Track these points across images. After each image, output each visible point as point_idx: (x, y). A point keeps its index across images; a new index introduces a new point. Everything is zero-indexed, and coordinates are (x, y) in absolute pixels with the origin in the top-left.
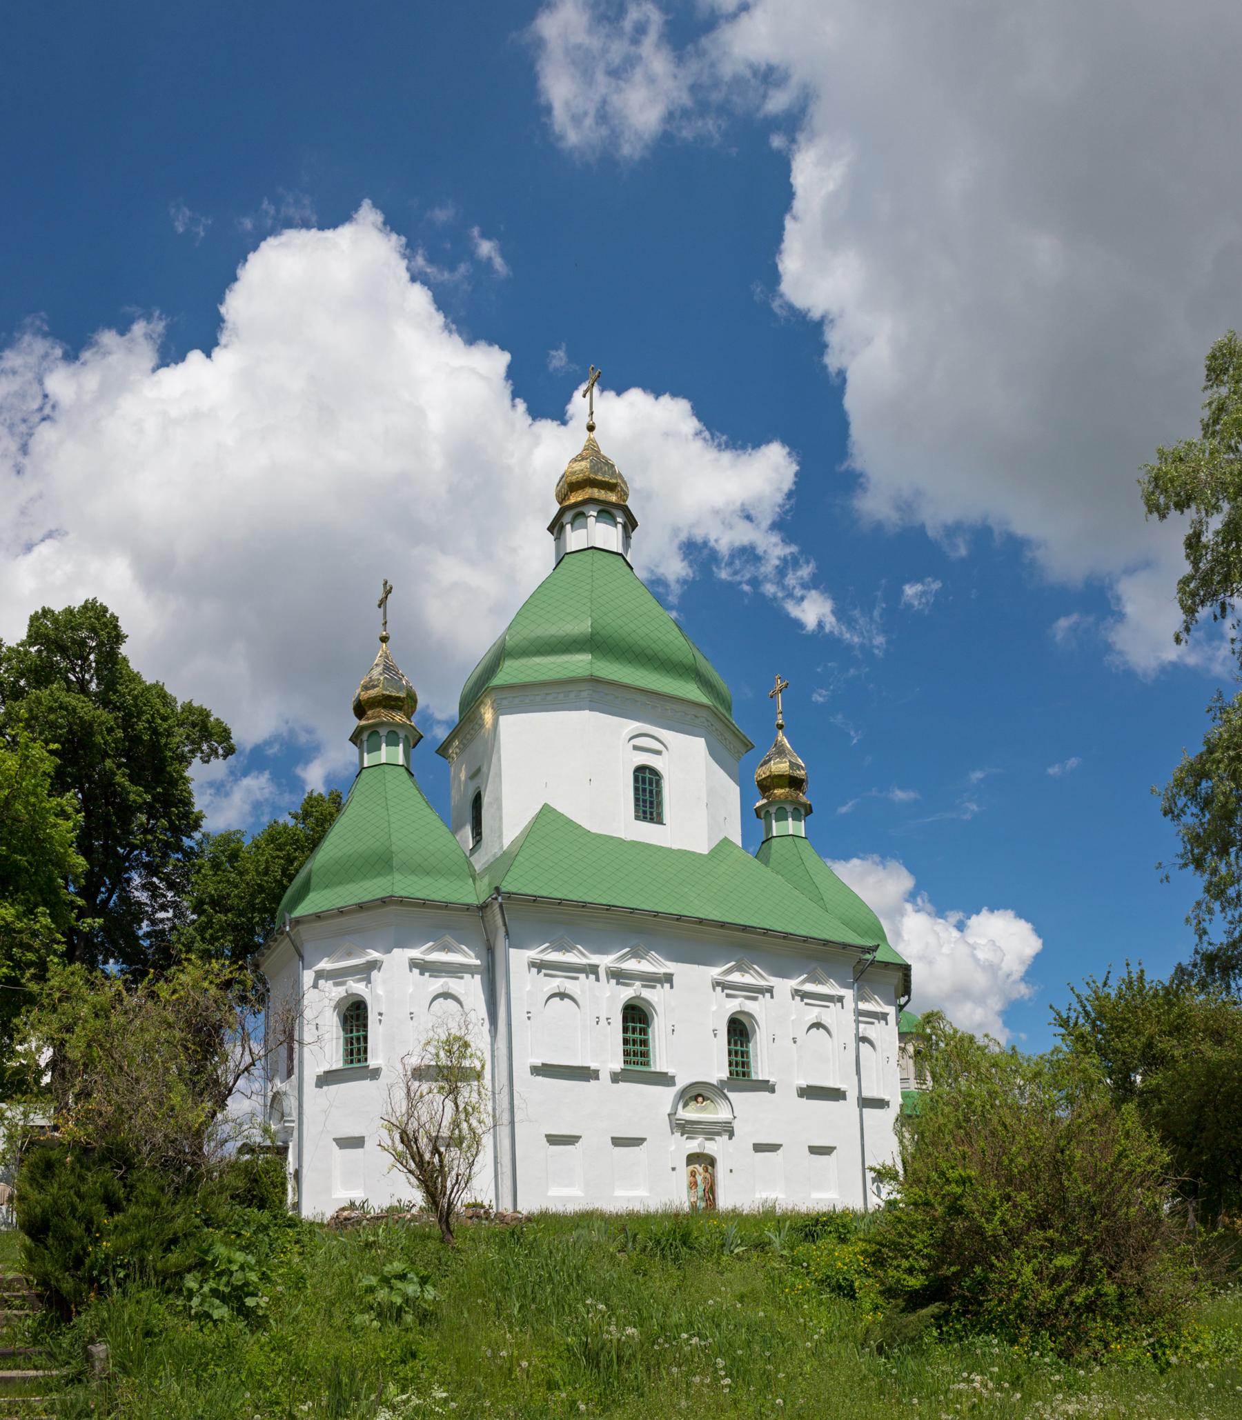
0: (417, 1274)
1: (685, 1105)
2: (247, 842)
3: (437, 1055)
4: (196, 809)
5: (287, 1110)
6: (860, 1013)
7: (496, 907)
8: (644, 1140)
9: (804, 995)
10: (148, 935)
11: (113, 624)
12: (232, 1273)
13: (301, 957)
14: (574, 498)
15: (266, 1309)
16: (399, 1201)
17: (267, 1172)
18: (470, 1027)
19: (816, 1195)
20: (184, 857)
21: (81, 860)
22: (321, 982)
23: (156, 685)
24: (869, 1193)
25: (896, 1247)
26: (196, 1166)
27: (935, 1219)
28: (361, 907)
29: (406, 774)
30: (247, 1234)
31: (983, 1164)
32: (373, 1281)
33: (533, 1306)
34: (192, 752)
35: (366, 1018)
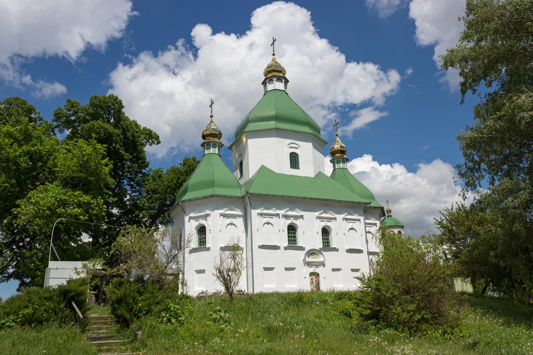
1: (308, 257)
2: (165, 171)
4: (147, 160)
6: (366, 224)
7: (247, 197)
9: (347, 219)
11: (120, 102)
13: (185, 212)
14: (269, 75)
22: (191, 220)
23: (134, 121)
28: (205, 197)
29: (218, 156)
30: (177, 300)
34: (146, 142)
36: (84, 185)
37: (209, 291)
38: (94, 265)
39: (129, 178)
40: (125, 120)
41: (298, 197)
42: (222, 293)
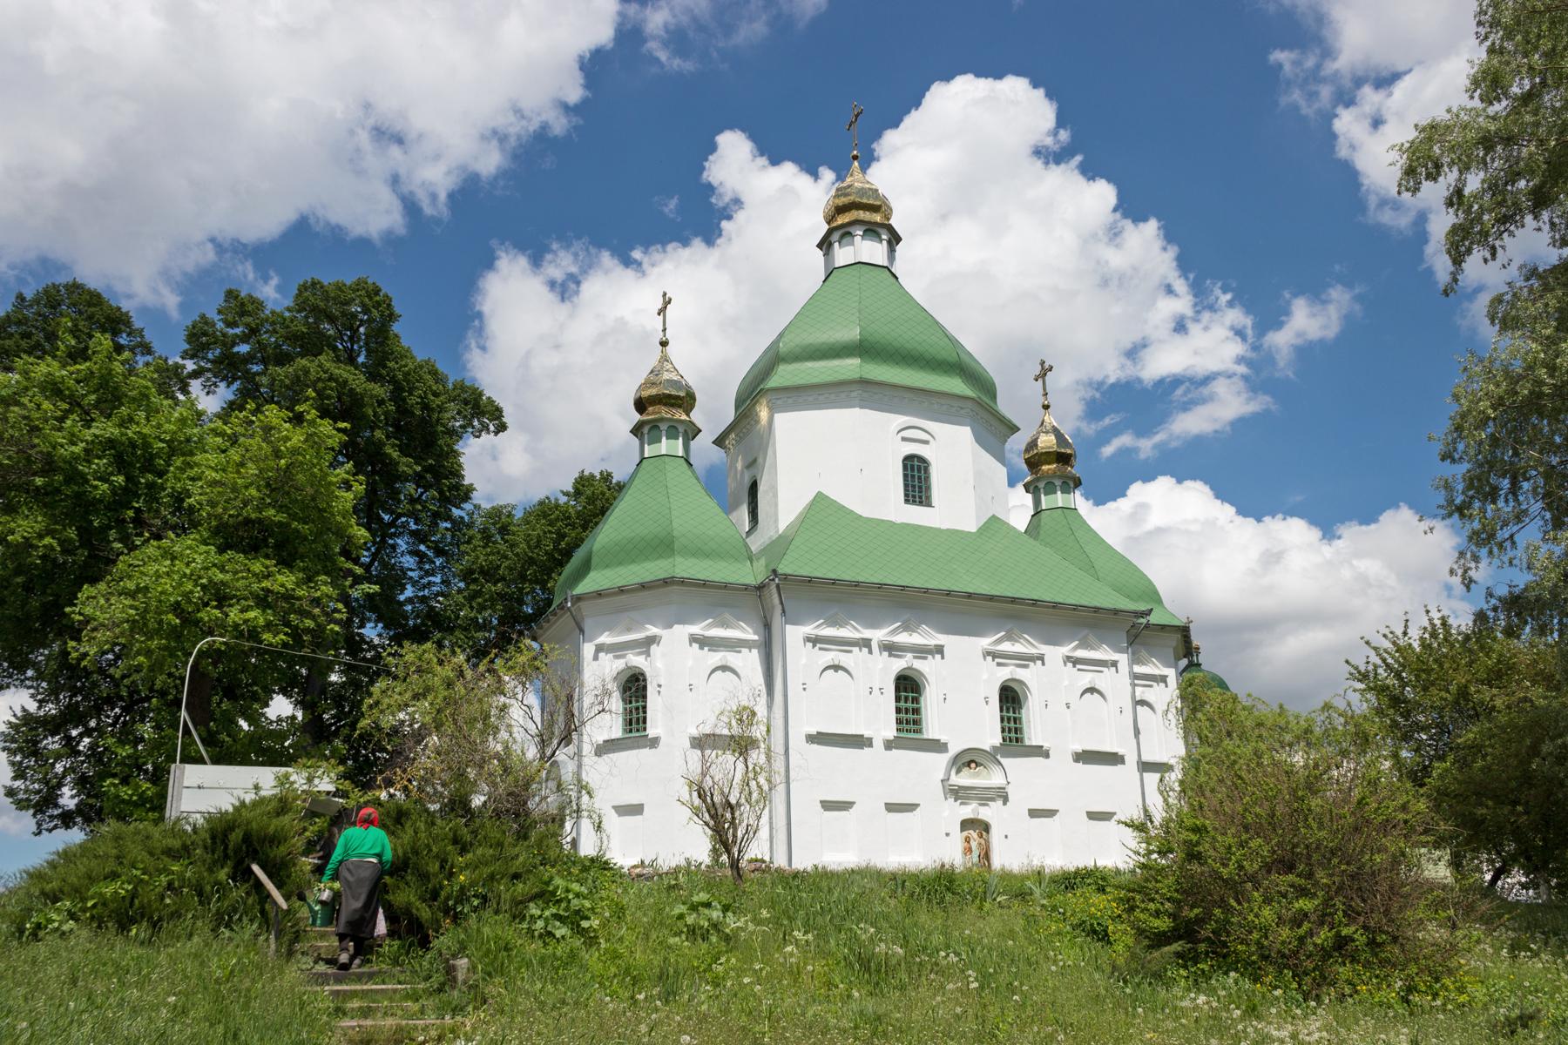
1: (958, 771)
2: (518, 514)
4: (466, 482)
6: (1136, 676)
9: (1076, 661)
13: (582, 631)
14: (841, 220)
21: (363, 532)
28: (643, 586)
36: (279, 547)
37: (660, 861)
38: (310, 780)
39: (413, 533)
40: (402, 357)
41: (927, 590)
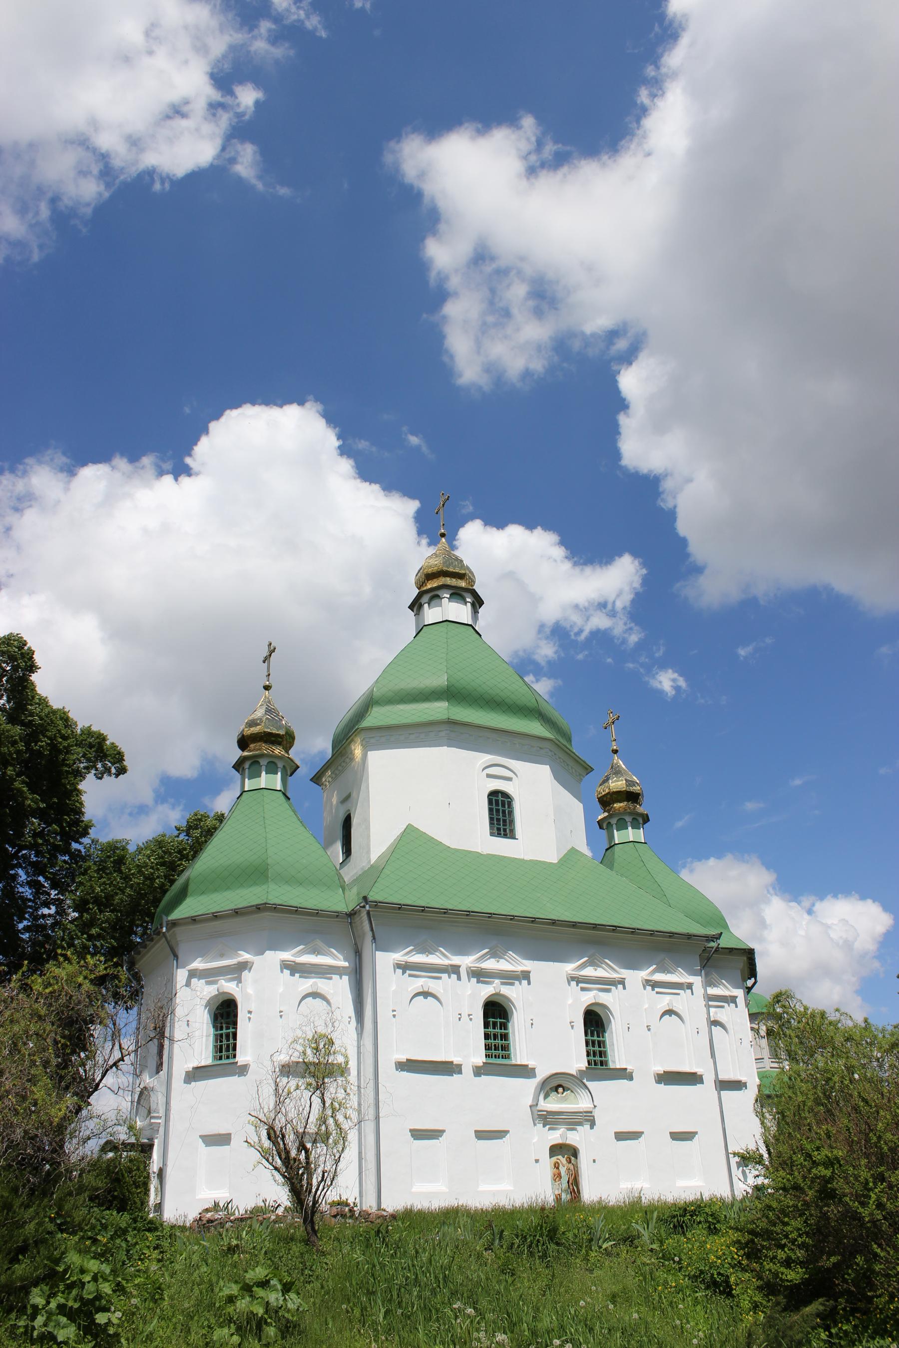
0: (280, 1281)
1: (546, 1097)
3: (304, 1053)
4: (86, 818)
5: (153, 1106)
6: (710, 998)
8: (507, 1132)
9: (654, 985)
10: (27, 929)
12: (83, 1284)
13: (176, 956)
15: (119, 1326)
16: (264, 1201)
17: (130, 1171)
18: (336, 1024)
19: (681, 1183)
20: (71, 859)
24: (735, 1179)
25: (767, 1234)
26: (55, 1164)
27: (806, 1204)
28: (237, 912)
30: (103, 1239)
31: (851, 1143)
32: (234, 1289)
33: (400, 1311)
35: (236, 1016)
39: (34, 865)
41: (513, 918)
42: (280, 1211)
